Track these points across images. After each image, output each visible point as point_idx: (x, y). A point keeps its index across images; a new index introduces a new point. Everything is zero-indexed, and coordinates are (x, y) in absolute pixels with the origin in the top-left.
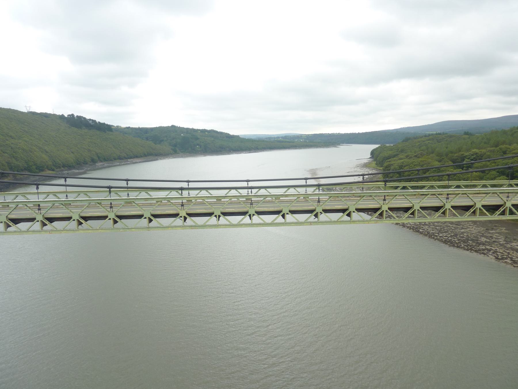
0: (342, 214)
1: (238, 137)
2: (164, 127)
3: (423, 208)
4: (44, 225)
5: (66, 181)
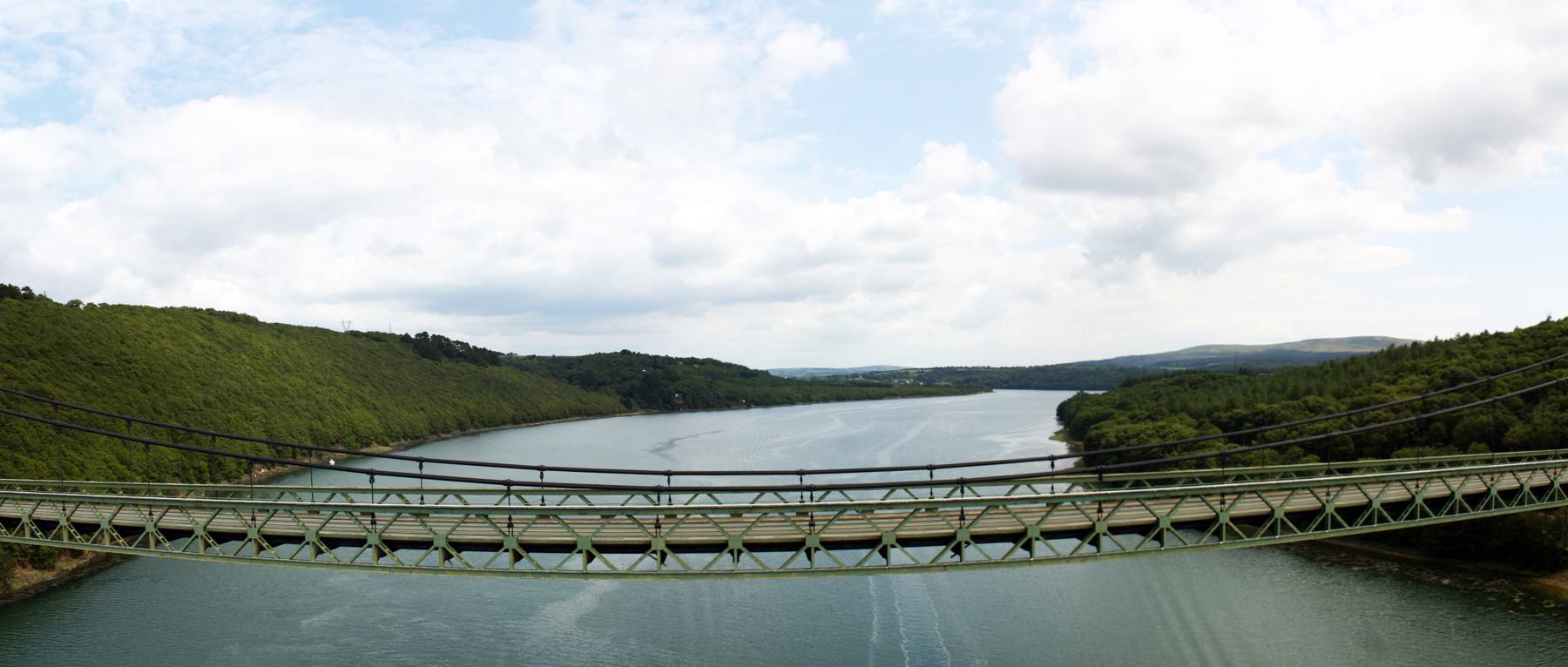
0: (1011, 545)
1: (766, 373)
2: (605, 355)
3: (1178, 525)
4: (381, 554)
5: (372, 481)
